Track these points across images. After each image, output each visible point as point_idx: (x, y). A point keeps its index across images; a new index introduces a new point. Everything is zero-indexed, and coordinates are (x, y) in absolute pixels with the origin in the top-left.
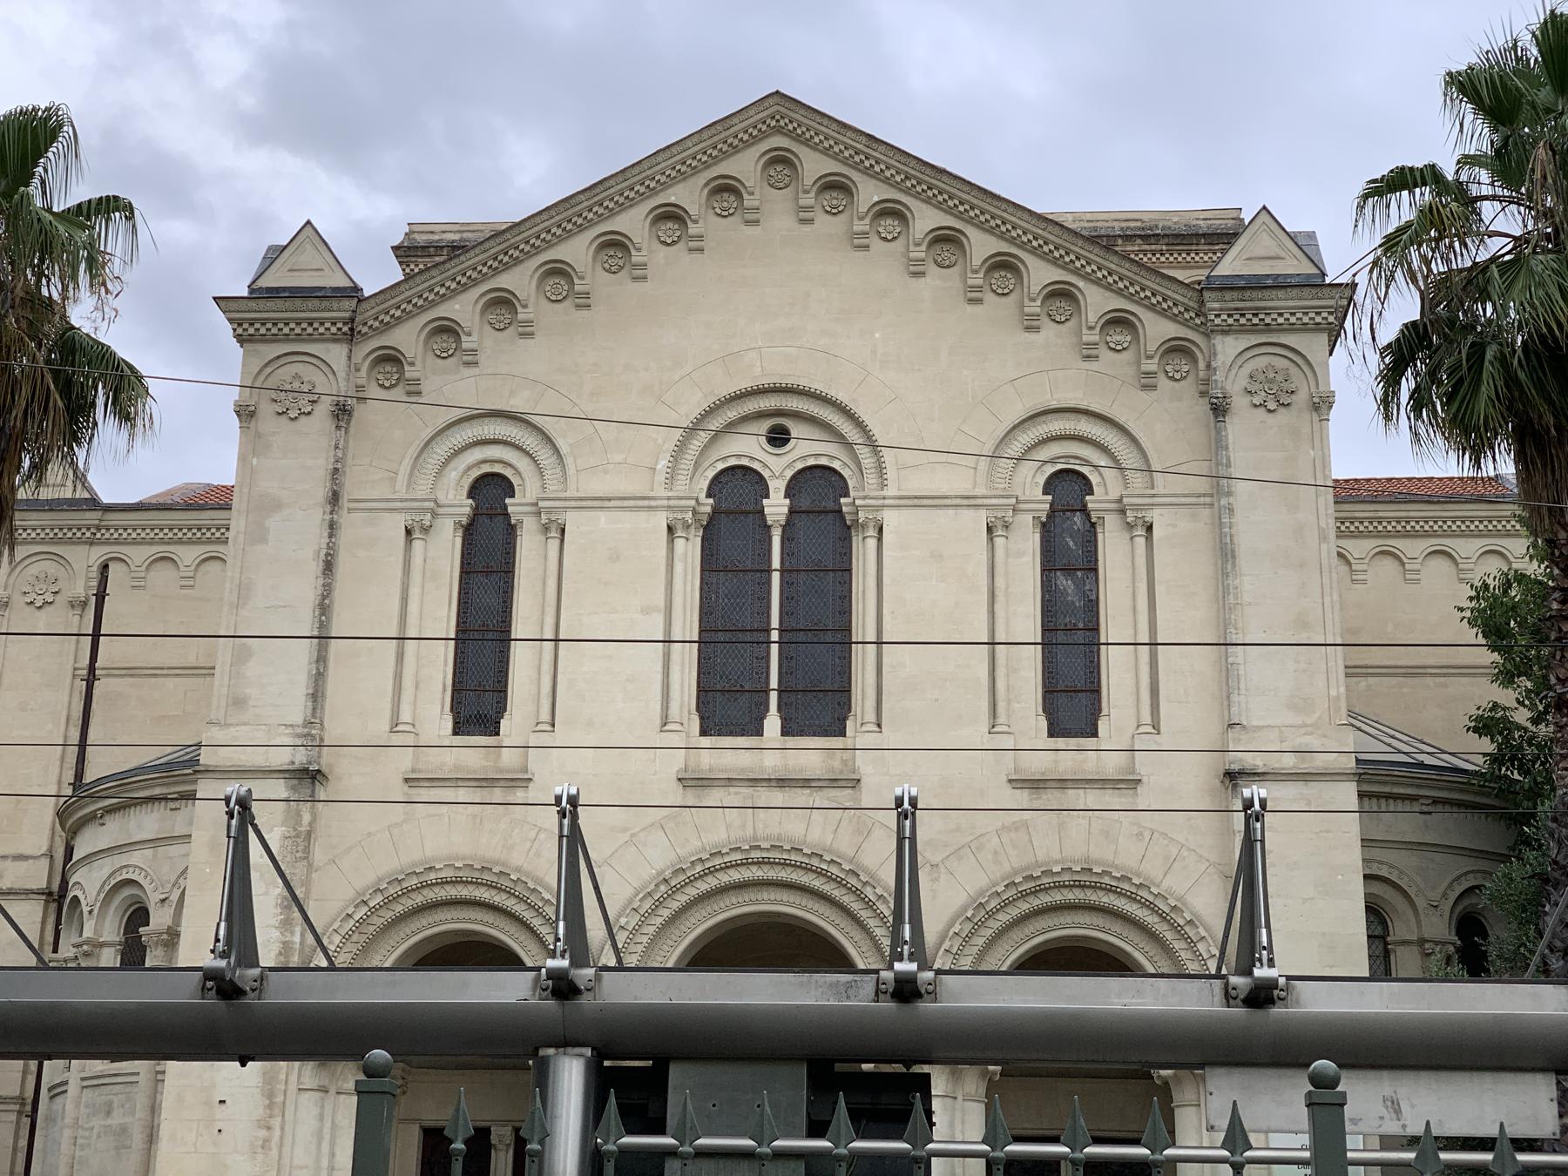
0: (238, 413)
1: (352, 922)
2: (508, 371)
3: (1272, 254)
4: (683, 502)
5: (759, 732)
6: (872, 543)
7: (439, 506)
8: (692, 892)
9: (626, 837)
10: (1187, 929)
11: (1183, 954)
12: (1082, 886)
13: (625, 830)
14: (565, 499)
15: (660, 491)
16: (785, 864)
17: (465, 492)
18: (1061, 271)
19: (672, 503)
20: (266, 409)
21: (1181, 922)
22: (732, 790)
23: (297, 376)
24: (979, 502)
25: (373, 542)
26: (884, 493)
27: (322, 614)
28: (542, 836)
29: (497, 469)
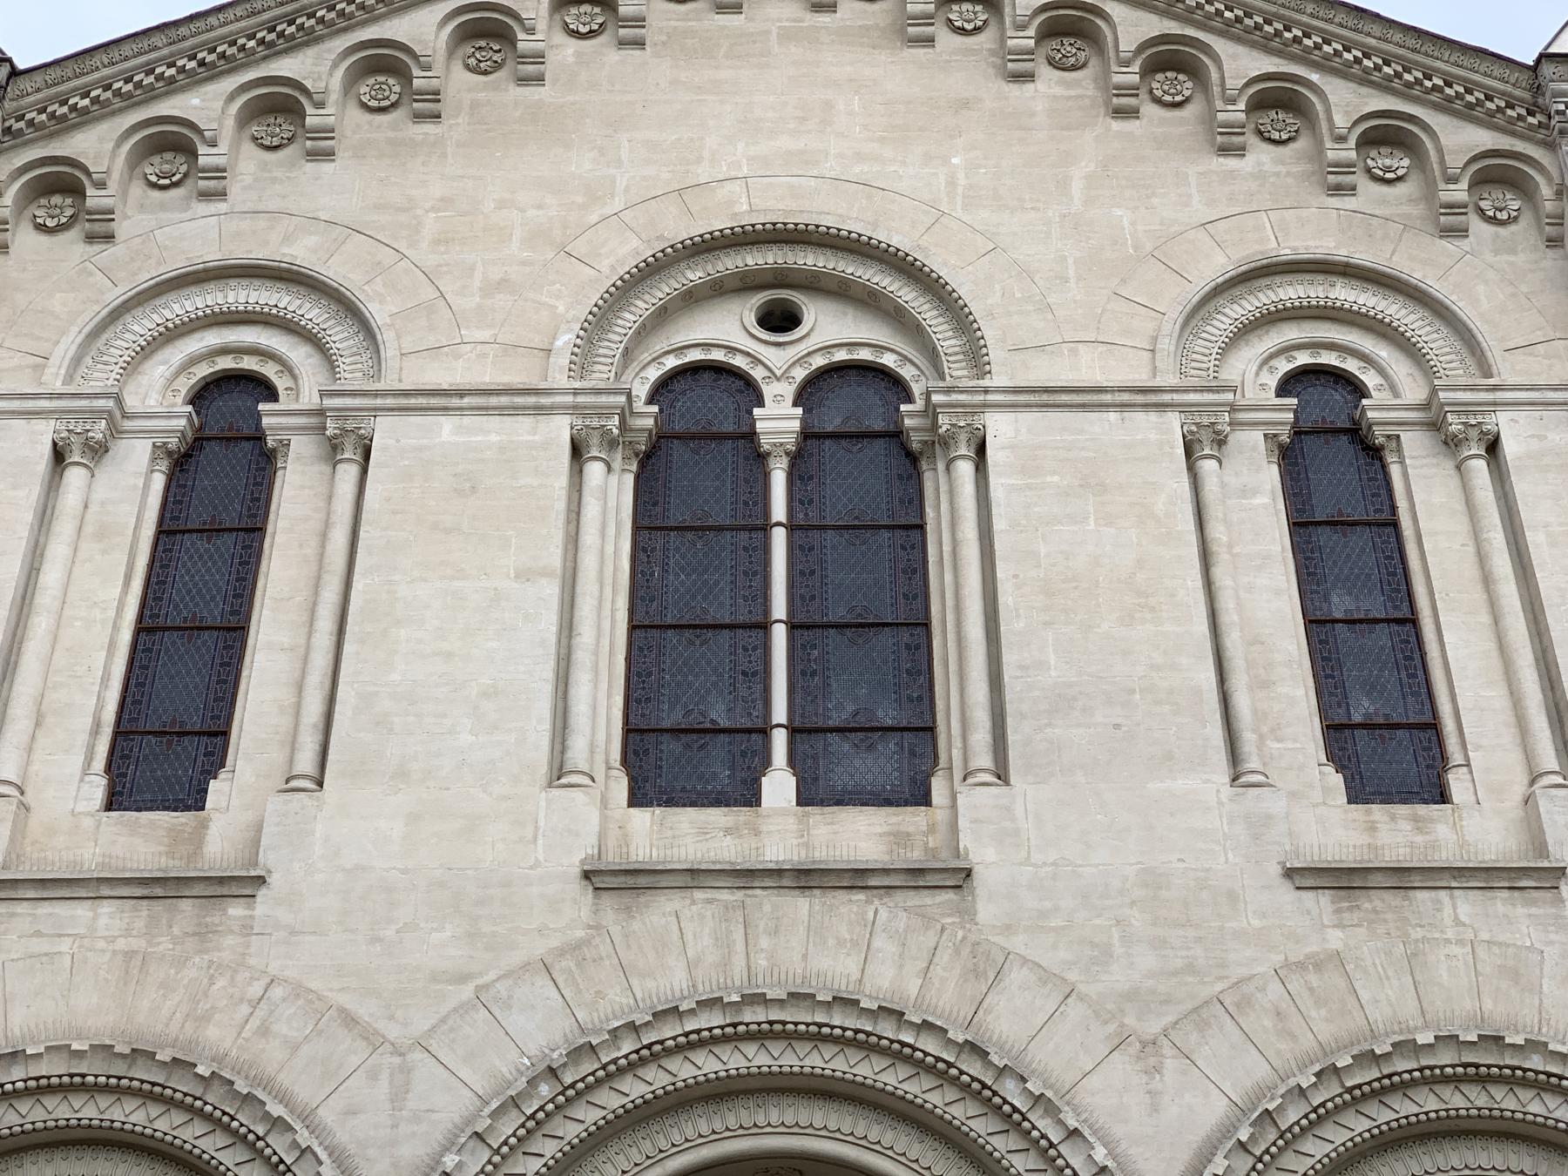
4: (603, 399)
5: (752, 798)
6: (965, 469)
7: (125, 416)
8: (611, 1101)
9: (467, 991)
12: (1481, 1078)
13: (463, 978)
15: (561, 380)
18: (1277, 60)
19: (581, 399)
22: (699, 895)
24: (1167, 398)
26: (986, 382)
28: (277, 992)
29: (249, 363)
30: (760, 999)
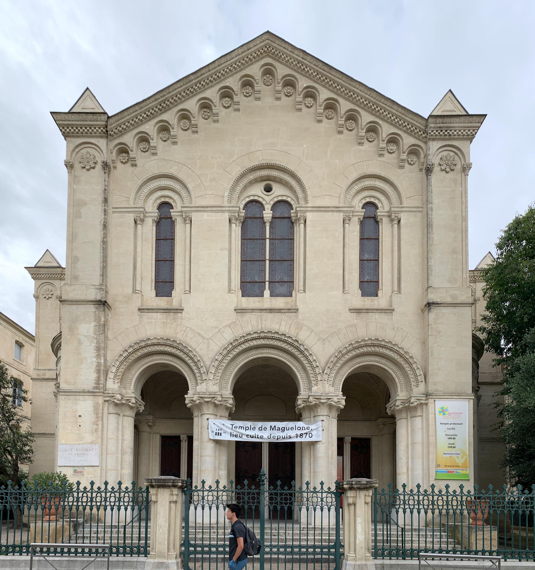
0: (66, 165)
1: (123, 358)
2: (168, 157)
3: (452, 109)
4: (235, 209)
5: (262, 296)
6: (302, 226)
10: (410, 360)
11: (407, 369)
13: (216, 328)
14: (191, 207)
16: (272, 338)
17: (156, 208)
20: (77, 166)
21: (408, 357)
22: (254, 313)
23: (88, 152)
24: (341, 209)
25: (122, 223)
26: (307, 205)
27: (104, 244)
30: (263, 332)
